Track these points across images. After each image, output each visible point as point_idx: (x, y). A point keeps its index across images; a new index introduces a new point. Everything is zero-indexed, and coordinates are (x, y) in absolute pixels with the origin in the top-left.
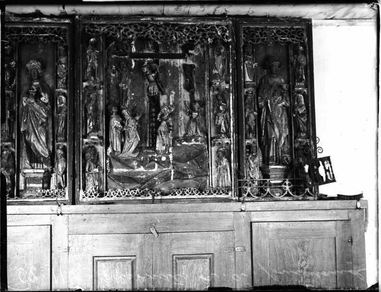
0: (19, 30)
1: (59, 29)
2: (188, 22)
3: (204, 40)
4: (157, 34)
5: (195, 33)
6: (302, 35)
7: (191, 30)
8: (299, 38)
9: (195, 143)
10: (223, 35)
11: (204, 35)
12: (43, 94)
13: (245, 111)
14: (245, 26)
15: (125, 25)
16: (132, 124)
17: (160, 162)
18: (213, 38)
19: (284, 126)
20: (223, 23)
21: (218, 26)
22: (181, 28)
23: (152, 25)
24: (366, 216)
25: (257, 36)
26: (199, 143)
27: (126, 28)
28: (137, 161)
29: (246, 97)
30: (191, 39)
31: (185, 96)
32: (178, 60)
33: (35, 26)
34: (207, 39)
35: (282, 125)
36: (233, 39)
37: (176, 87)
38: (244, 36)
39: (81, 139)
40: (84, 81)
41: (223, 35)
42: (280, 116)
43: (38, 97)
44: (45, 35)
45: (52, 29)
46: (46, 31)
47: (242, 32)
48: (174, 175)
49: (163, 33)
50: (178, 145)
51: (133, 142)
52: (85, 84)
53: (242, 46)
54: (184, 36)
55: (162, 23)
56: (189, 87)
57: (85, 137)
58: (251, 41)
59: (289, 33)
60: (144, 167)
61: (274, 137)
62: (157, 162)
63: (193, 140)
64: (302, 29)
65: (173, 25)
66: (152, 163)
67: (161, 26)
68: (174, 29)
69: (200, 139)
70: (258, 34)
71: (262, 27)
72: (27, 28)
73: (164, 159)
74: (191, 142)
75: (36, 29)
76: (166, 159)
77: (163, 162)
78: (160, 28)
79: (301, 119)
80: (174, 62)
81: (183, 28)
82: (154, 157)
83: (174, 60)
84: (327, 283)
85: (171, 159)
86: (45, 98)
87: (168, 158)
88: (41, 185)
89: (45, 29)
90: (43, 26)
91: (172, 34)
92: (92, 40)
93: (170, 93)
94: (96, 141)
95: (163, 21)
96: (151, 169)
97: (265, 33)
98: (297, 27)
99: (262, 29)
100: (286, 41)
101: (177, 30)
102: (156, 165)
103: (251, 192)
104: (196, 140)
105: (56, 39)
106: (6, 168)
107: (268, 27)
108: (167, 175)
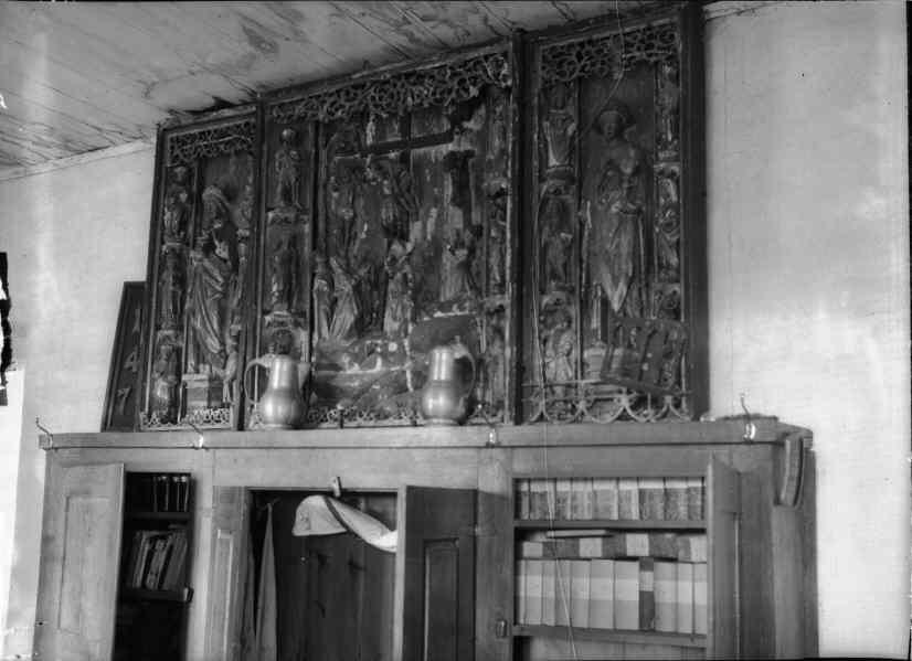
0: (193, 137)
1: (247, 124)
2: (433, 62)
3: (462, 92)
4: (380, 99)
5: (445, 82)
6: (672, 37)
7: (438, 77)
8: (665, 45)
9: (459, 313)
10: (497, 75)
11: (462, 81)
12: (217, 243)
13: (540, 231)
14: (546, 47)
15: (331, 95)
16: (345, 286)
17: (385, 355)
18: (480, 85)
19: (624, 257)
20: (497, 49)
21: (486, 58)
22: (420, 77)
23: (374, 83)
24: (107, 416)
25: (570, 63)
26: (467, 312)
27: (332, 99)
28: (350, 354)
29: (544, 202)
30: (438, 96)
31: (456, 218)
32: (444, 146)
33: (216, 127)
34: (467, 90)
35: (618, 255)
36: (514, 79)
37: (437, 201)
38: (543, 68)
39: (259, 317)
40: (268, 210)
41: (497, 75)
42: (611, 235)
43: (209, 249)
44: (227, 139)
45: (238, 126)
46: (229, 132)
47: (540, 58)
48: (412, 379)
49: (392, 96)
50: (426, 319)
51: (346, 316)
52: (271, 215)
53: (536, 91)
54: (426, 92)
55: (388, 76)
56: (461, 199)
57: (265, 312)
58: (557, 77)
59: (642, 41)
60: (360, 364)
61: (596, 285)
62: (381, 354)
63: (455, 307)
64: (672, 24)
65: (408, 76)
66: (372, 356)
67: (387, 82)
68: (409, 83)
69: (467, 304)
70: (574, 58)
71: (581, 40)
72: (203, 133)
73: (393, 347)
74: (450, 310)
75: (215, 131)
76: (398, 349)
77: (393, 354)
78: (387, 86)
79: (665, 239)
80: (436, 152)
81: (423, 77)
82: (376, 345)
83: (437, 147)
84: (898, 652)
85: (407, 349)
86: (222, 250)
87: (401, 346)
88: (205, 403)
89: (228, 128)
90: (226, 124)
91: (405, 93)
92: (285, 133)
93: (427, 215)
94: (284, 319)
95: (391, 71)
96: (370, 368)
97: (588, 53)
98: (661, 22)
99: (582, 45)
100: (633, 61)
101: (415, 84)
102: (379, 362)
103: (547, 410)
104: (461, 308)
105: (244, 142)
106: (162, 374)
107: (595, 37)
108: (396, 381)
